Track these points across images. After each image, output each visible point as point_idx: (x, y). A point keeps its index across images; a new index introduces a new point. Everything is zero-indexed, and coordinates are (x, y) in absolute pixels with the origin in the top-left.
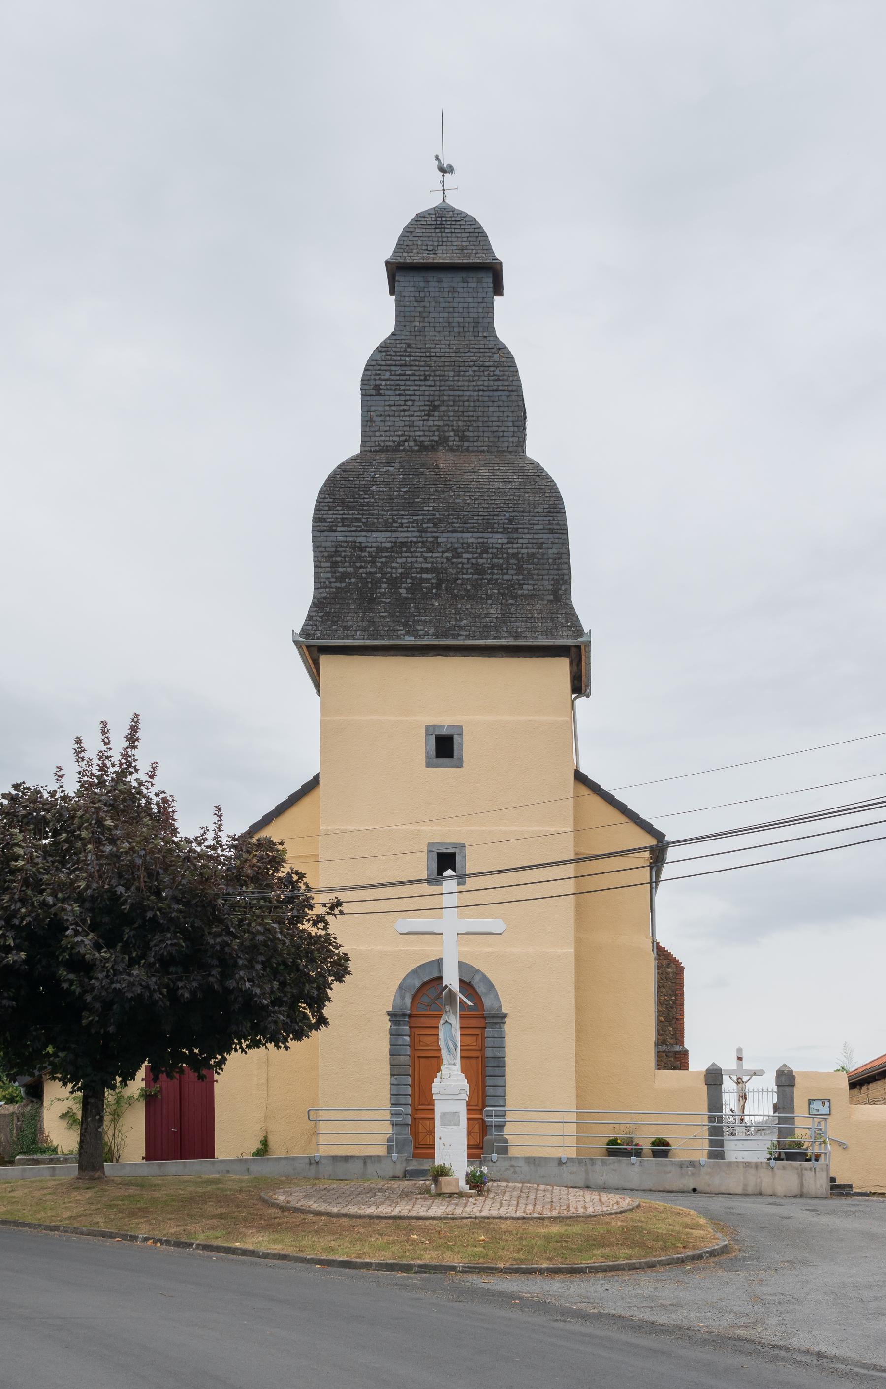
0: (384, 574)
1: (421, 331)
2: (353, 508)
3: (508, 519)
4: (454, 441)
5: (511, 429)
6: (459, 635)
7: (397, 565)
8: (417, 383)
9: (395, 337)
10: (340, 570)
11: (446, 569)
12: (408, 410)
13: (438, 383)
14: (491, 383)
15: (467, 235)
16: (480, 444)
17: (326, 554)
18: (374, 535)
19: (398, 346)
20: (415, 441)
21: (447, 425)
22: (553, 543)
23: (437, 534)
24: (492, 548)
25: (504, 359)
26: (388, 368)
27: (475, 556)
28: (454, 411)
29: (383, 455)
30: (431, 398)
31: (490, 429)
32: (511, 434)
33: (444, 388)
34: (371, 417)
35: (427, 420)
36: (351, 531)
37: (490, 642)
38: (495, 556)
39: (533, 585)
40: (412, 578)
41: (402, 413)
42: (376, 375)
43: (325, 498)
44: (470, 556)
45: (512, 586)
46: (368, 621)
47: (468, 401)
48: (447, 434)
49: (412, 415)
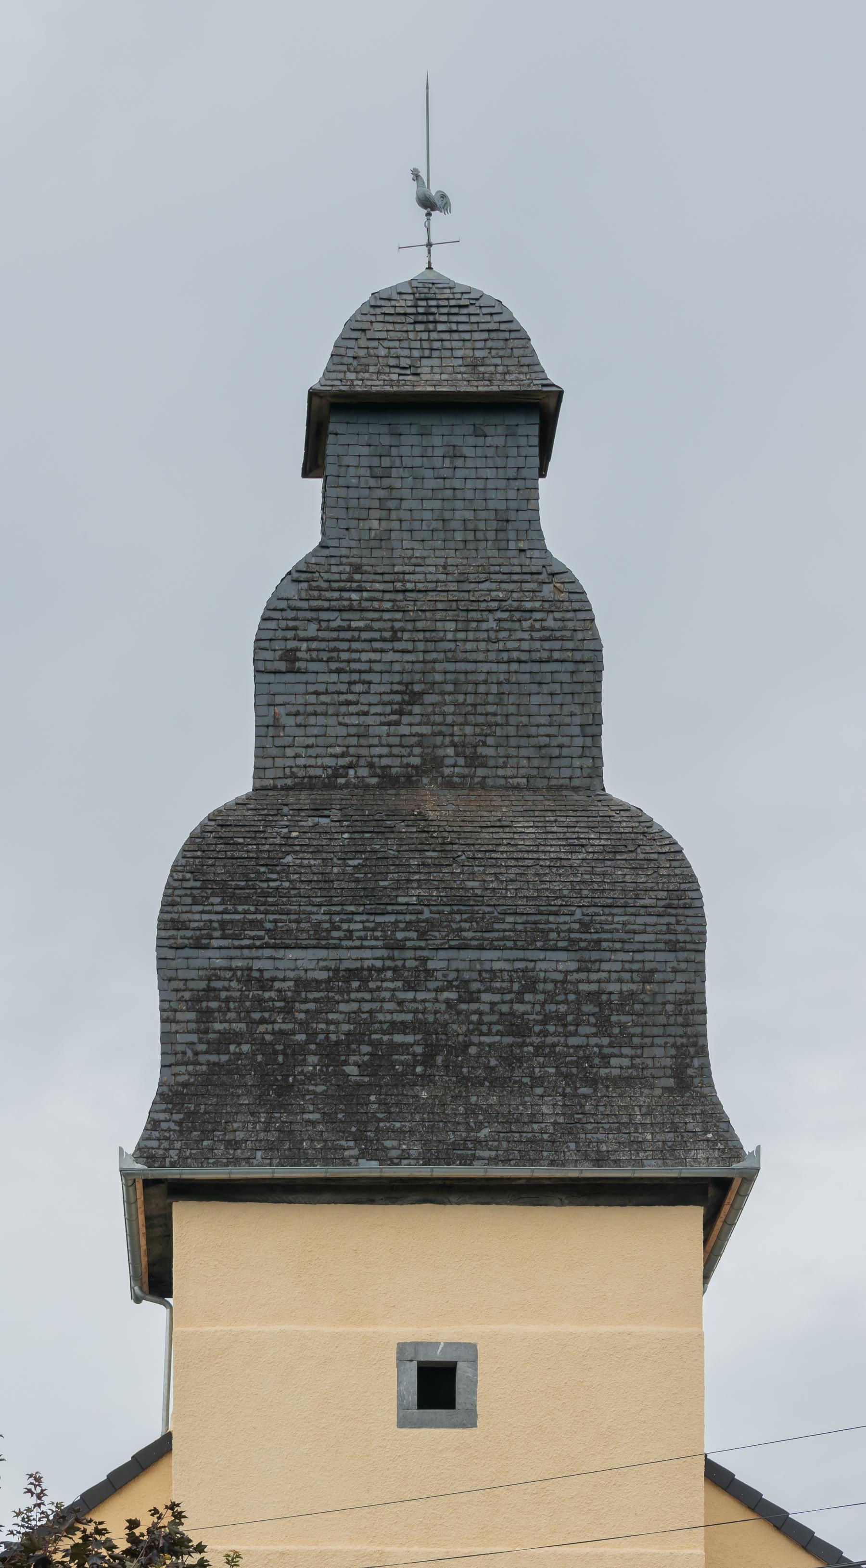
0: (312, 1035)
1: (384, 538)
2: (246, 900)
3: (580, 922)
4: (455, 765)
5: (579, 741)
6: (474, 1158)
7: (340, 1017)
8: (376, 645)
9: (326, 552)
10: (218, 1026)
11: (445, 1025)
12: (356, 703)
13: (421, 646)
14: (537, 645)
15: (485, 335)
16: (509, 772)
17: (187, 995)
18: (291, 954)
19: (334, 569)
20: (371, 766)
21: (440, 733)
22: (675, 971)
23: (425, 953)
24: (545, 981)
25: (564, 596)
26: (313, 615)
27: (508, 997)
28: (456, 704)
29: (304, 795)
30: (406, 678)
31: (533, 741)
32: (579, 751)
33: (434, 656)
34: (276, 718)
35: (397, 723)
36: (242, 947)
37: (542, 1172)
38: (550, 997)
39: (632, 1057)
40: (371, 1043)
41: (343, 709)
42: (288, 629)
43: (183, 880)
44: (497, 998)
45: (587, 1058)
46: (279, 1130)
47: (485, 682)
48: (440, 752)
49: (366, 714)
